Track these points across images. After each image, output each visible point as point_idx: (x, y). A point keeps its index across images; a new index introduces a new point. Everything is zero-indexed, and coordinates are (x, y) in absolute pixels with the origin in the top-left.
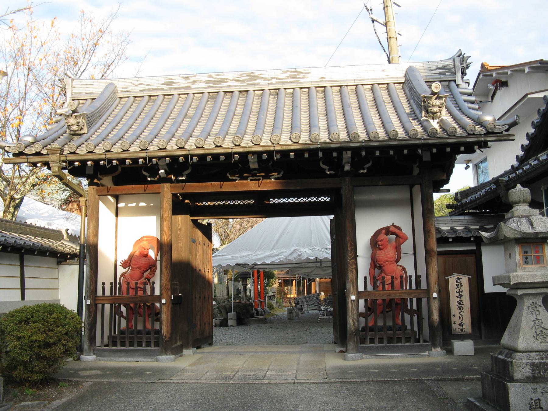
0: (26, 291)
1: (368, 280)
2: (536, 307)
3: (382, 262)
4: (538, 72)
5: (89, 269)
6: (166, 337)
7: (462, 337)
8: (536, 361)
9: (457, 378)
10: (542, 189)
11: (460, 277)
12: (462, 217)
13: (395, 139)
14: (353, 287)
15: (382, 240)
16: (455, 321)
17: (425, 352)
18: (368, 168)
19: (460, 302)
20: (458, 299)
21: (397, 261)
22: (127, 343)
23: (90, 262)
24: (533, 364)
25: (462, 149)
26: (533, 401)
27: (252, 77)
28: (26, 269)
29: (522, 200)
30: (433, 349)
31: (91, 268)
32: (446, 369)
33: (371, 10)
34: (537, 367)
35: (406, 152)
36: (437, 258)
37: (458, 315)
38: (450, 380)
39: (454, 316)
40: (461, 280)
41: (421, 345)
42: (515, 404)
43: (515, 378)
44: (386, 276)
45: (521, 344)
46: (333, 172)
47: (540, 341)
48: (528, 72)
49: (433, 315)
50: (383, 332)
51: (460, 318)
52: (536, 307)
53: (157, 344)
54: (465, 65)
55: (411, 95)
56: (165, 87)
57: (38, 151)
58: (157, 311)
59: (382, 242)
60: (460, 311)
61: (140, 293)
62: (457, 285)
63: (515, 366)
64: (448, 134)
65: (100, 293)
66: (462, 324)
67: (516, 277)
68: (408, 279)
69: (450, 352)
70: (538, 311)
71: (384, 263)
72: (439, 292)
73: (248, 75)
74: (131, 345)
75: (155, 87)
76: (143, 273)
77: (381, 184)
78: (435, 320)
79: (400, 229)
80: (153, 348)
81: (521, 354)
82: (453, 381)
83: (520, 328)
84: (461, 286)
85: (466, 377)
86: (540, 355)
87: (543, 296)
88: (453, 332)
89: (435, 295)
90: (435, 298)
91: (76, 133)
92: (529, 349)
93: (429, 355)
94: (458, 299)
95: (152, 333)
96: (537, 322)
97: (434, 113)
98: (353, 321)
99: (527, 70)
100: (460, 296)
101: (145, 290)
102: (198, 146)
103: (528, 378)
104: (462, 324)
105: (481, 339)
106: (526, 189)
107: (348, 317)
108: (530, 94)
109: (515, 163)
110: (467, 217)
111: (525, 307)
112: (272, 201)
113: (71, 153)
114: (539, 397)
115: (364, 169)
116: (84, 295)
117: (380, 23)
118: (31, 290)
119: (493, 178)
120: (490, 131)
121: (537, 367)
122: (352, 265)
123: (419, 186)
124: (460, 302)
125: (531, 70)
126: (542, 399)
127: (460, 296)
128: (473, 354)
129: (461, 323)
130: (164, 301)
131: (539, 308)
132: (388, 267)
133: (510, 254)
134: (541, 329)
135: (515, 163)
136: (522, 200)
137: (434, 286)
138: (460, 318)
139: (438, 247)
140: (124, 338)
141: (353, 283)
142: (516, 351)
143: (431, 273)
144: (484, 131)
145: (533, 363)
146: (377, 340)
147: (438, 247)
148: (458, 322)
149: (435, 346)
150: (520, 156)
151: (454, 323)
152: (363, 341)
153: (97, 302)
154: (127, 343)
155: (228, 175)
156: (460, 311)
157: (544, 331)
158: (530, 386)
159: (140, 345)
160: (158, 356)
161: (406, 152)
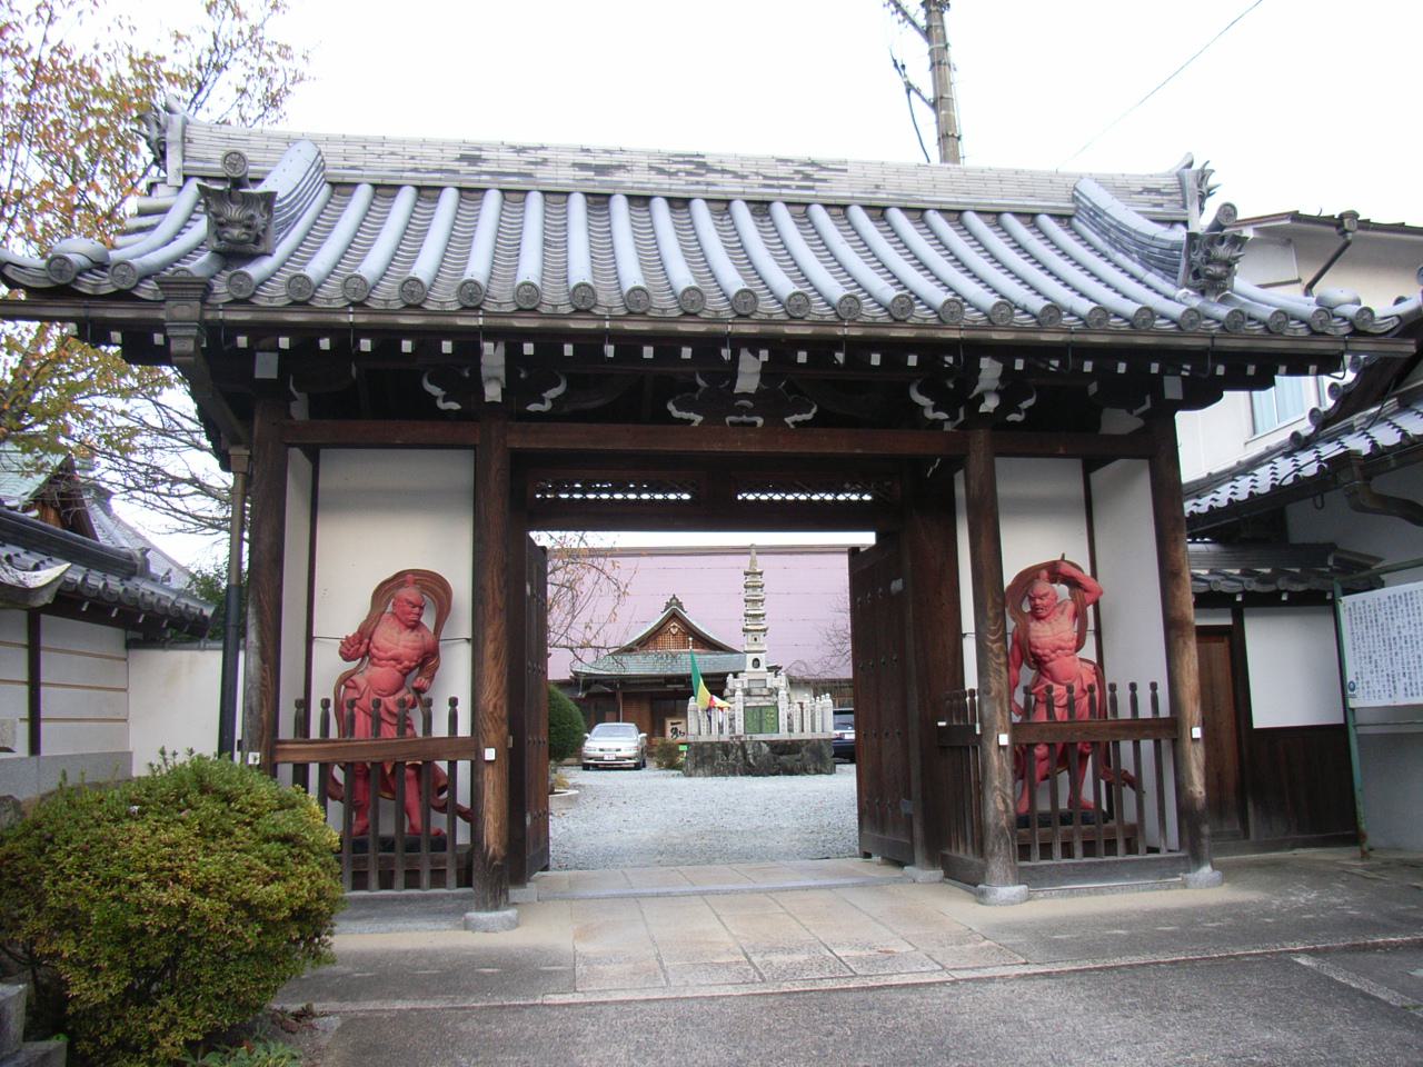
0: (44, 726)
1: (331, 710)
3: (1047, 651)
5: (255, 660)
6: (494, 858)
14: (1002, 711)
15: (1046, 595)
18: (1028, 410)
21: (1078, 648)
22: (374, 879)
23: (261, 638)
27: (700, 165)
28: (46, 660)
31: (264, 658)
33: (903, 66)
36: (1198, 642)
44: (1055, 686)
46: (455, 406)
49: (1191, 783)
50: (1071, 827)
53: (465, 880)
54: (1204, 190)
55: (1113, 243)
56: (464, 167)
57: (124, 287)
58: (443, 782)
59: (1045, 602)
61: (389, 732)
65: (286, 730)
68: (1108, 693)
71: (1053, 652)
72: (1204, 725)
73: (687, 159)
74: (386, 883)
75: (432, 165)
76: (405, 675)
77: (1061, 451)
78: (1198, 795)
79: (1080, 569)
80: (1058, 860)
89: (1197, 733)
91: (239, 248)
93: (1185, 885)
95: (398, 845)
98: (1004, 801)
101: (404, 724)
102: (632, 309)
105: (1247, 836)
107: (988, 794)
109: (1306, 428)
112: (246, 567)
113: (236, 301)
115: (542, 401)
116: (238, 736)
117: (924, 99)
118: (75, 724)
119: (1239, 463)
120: (1361, 328)
122: (998, 657)
130: (490, 754)
132: (1058, 664)
135: (1306, 428)
139: (1197, 616)
140: (390, 861)
141: (1001, 704)
143: (1186, 679)
144: (1344, 329)
146: (1057, 851)
147: (1197, 616)
152: (1024, 852)
153: (279, 758)
154: (374, 879)
155: (671, 407)
159: (1046, 851)
160: (469, 915)
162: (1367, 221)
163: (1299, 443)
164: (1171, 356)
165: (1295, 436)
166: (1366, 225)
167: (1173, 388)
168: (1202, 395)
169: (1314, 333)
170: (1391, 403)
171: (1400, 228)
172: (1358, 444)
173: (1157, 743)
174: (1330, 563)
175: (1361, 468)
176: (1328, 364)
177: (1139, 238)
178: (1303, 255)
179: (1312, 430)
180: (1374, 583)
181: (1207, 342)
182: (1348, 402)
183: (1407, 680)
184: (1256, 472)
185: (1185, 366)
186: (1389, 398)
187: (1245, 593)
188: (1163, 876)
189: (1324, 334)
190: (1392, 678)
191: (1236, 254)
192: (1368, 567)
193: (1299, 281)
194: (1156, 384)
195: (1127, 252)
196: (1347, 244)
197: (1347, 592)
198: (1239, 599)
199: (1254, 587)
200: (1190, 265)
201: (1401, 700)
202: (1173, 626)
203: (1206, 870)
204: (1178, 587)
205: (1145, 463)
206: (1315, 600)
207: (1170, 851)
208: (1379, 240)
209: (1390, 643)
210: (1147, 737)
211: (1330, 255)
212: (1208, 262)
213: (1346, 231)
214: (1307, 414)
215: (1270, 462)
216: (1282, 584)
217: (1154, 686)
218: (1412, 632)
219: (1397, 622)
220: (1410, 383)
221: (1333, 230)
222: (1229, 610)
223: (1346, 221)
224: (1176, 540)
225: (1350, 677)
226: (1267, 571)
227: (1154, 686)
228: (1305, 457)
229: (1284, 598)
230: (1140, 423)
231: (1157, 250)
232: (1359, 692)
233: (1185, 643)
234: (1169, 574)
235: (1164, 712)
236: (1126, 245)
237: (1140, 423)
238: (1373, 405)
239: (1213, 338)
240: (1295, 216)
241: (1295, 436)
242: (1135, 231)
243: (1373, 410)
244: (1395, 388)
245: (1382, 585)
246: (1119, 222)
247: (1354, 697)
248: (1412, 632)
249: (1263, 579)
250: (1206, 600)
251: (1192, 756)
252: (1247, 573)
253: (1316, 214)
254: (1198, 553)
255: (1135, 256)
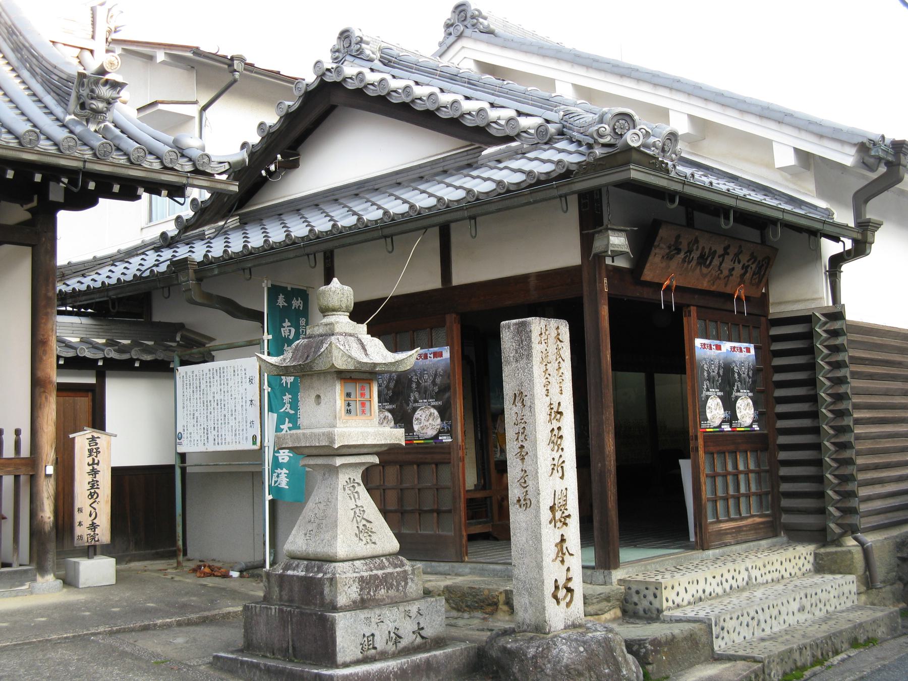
2: (353, 486)
4: (176, 67)
7: (91, 551)
8: (365, 574)
9: (145, 626)
10: (264, 285)
11: (96, 435)
12: (75, 320)
13: (32, 148)
16: (82, 520)
17: (22, 585)
19: (94, 485)
20: (90, 478)
24: (362, 580)
25: (116, 188)
26: (366, 639)
29: (344, 306)
30: (39, 578)
32: (67, 616)
34: (367, 584)
35: (10, 174)
36: (57, 396)
37: (87, 510)
38: (132, 630)
39: (80, 510)
40: (98, 441)
41: (16, 572)
42: (343, 647)
43: (339, 605)
45: (341, 550)
47: (364, 542)
48: (163, 62)
49: (43, 510)
51: (90, 515)
52: (353, 486)
55: (23, 60)
60: (92, 500)
62: (90, 451)
63: (339, 585)
64: (129, 160)
66: (93, 526)
67: (342, 435)
69: (69, 581)
70: (356, 492)
72: (57, 463)
78: (47, 520)
81: (341, 564)
82: (139, 631)
83: (336, 521)
84: (98, 452)
85: (159, 622)
86: (366, 564)
87: (363, 468)
88: (77, 543)
89: (50, 470)
90: (50, 476)
92: (352, 556)
94: (90, 478)
96: (357, 511)
97: (97, 112)
99: (161, 56)
100: (94, 472)
103: (354, 602)
104: (93, 526)
106: (346, 288)
108: (162, 102)
109: (172, 229)
110: (84, 320)
111: (340, 487)
114: (373, 631)
119: (119, 251)
120: (201, 168)
121: (367, 584)
123: (29, 249)
124: (94, 485)
125: (168, 60)
126: (377, 633)
127: (94, 472)
128: (113, 582)
129: (93, 523)
131: (358, 489)
133: (318, 397)
134: (364, 522)
135: (172, 229)
136: (344, 306)
137: (48, 453)
138: (90, 515)
139: (58, 375)
142: (332, 560)
143: (45, 426)
144: (189, 167)
145: (362, 577)
147: (58, 375)
148: (87, 522)
149: (42, 569)
150: (185, 218)
151: (80, 524)
156: (92, 500)
157: (368, 525)
158: (362, 615)
161: (10, 174)
162: (252, 65)
163: (166, 242)
164: (53, 172)
165: (164, 235)
166: (250, 67)
167: (56, 193)
168: (81, 200)
169: (165, 168)
170: (233, 221)
171: (276, 75)
172: (198, 253)
173: (17, 478)
174: (178, 339)
175: (195, 271)
176: (176, 191)
177: (44, 63)
178: (202, 83)
179: (176, 232)
180: (207, 357)
181: (79, 164)
182: (205, 214)
183: (215, 433)
184: (130, 261)
185: (63, 179)
186: (233, 216)
187: (105, 359)
188: (13, 586)
189: (172, 169)
190: (206, 431)
191: (115, 95)
192: (203, 345)
193: (196, 103)
194: (42, 190)
195: (33, 74)
196: (235, 81)
197: (184, 363)
198: (100, 363)
199: (113, 354)
200: (79, 97)
201: (211, 448)
202: (37, 384)
203: (50, 578)
204: (45, 352)
205: (29, 250)
206: (160, 368)
207: (21, 565)
208: (261, 80)
209: (206, 404)
210: (9, 473)
211: (223, 85)
212: (92, 98)
213: (235, 71)
214: (174, 217)
215: (143, 253)
216: (134, 354)
217: (18, 432)
218: (222, 397)
219: (213, 389)
220: (263, 203)
221: (226, 66)
222: (94, 372)
223: (235, 62)
224: (47, 314)
225: (179, 429)
226: (151, 343)
227: (18, 432)
228: (167, 254)
229: (137, 365)
230: (27, 216)
231: (56, 78)
232: (184, 441)
233: (46, 398)
234: (38, 344)
235: (25, 452)
236: (34, 67)
237: (27, 216)
238: (221, 220)
239: (85, 161)
240: (196, 51)
241: (164, 235)
242: (42, 57)
243: (221, 223)
244: (236, 210)
245: (212, 359)
246: (31, 46)
247: (180, 444)
248: (222, 397)
249: (122, 349)
250: (74, 363)
251: (45, 488)
252: (111, 343)
253: (214, 52)
254: (71, 329)
255: (38, 78)
